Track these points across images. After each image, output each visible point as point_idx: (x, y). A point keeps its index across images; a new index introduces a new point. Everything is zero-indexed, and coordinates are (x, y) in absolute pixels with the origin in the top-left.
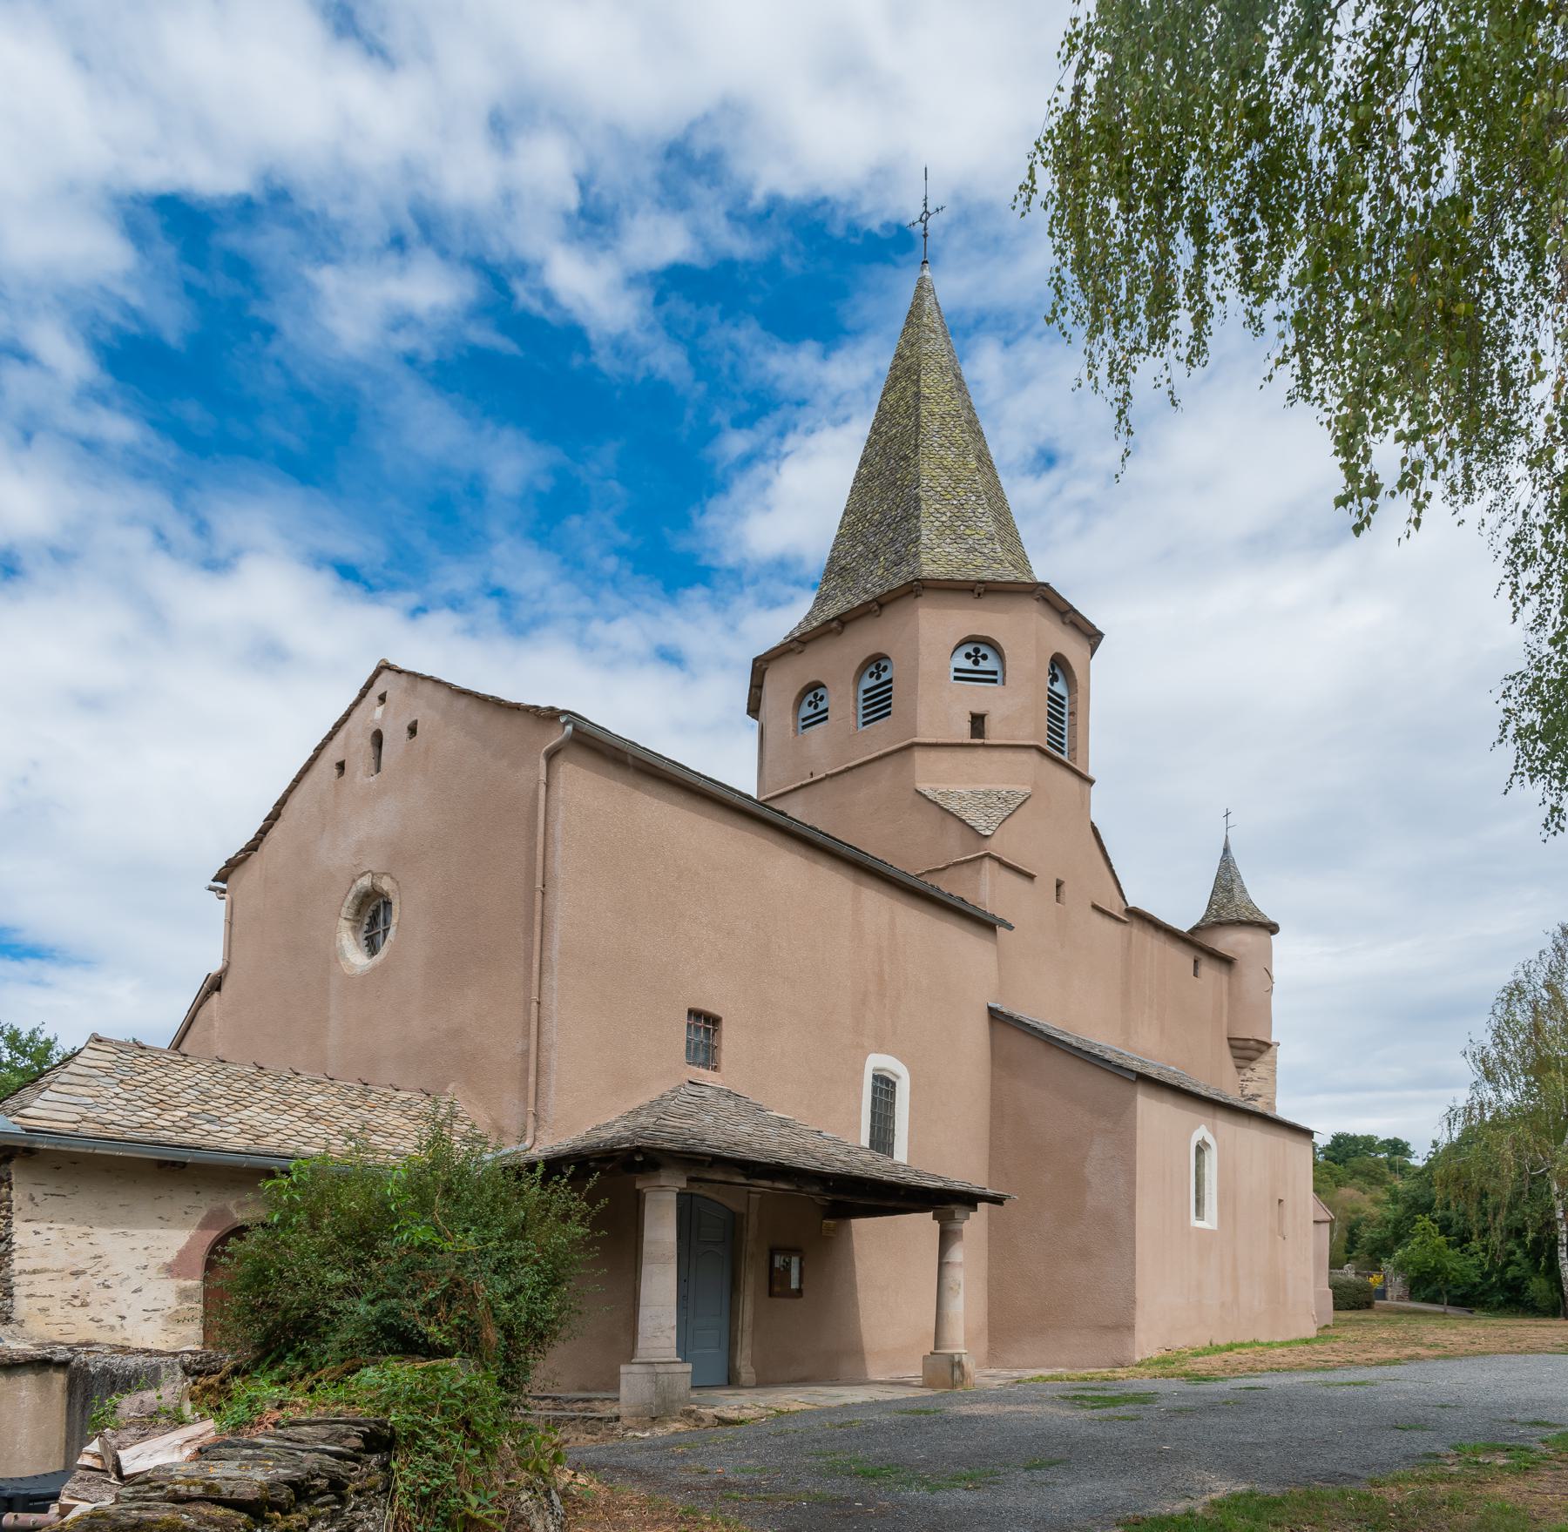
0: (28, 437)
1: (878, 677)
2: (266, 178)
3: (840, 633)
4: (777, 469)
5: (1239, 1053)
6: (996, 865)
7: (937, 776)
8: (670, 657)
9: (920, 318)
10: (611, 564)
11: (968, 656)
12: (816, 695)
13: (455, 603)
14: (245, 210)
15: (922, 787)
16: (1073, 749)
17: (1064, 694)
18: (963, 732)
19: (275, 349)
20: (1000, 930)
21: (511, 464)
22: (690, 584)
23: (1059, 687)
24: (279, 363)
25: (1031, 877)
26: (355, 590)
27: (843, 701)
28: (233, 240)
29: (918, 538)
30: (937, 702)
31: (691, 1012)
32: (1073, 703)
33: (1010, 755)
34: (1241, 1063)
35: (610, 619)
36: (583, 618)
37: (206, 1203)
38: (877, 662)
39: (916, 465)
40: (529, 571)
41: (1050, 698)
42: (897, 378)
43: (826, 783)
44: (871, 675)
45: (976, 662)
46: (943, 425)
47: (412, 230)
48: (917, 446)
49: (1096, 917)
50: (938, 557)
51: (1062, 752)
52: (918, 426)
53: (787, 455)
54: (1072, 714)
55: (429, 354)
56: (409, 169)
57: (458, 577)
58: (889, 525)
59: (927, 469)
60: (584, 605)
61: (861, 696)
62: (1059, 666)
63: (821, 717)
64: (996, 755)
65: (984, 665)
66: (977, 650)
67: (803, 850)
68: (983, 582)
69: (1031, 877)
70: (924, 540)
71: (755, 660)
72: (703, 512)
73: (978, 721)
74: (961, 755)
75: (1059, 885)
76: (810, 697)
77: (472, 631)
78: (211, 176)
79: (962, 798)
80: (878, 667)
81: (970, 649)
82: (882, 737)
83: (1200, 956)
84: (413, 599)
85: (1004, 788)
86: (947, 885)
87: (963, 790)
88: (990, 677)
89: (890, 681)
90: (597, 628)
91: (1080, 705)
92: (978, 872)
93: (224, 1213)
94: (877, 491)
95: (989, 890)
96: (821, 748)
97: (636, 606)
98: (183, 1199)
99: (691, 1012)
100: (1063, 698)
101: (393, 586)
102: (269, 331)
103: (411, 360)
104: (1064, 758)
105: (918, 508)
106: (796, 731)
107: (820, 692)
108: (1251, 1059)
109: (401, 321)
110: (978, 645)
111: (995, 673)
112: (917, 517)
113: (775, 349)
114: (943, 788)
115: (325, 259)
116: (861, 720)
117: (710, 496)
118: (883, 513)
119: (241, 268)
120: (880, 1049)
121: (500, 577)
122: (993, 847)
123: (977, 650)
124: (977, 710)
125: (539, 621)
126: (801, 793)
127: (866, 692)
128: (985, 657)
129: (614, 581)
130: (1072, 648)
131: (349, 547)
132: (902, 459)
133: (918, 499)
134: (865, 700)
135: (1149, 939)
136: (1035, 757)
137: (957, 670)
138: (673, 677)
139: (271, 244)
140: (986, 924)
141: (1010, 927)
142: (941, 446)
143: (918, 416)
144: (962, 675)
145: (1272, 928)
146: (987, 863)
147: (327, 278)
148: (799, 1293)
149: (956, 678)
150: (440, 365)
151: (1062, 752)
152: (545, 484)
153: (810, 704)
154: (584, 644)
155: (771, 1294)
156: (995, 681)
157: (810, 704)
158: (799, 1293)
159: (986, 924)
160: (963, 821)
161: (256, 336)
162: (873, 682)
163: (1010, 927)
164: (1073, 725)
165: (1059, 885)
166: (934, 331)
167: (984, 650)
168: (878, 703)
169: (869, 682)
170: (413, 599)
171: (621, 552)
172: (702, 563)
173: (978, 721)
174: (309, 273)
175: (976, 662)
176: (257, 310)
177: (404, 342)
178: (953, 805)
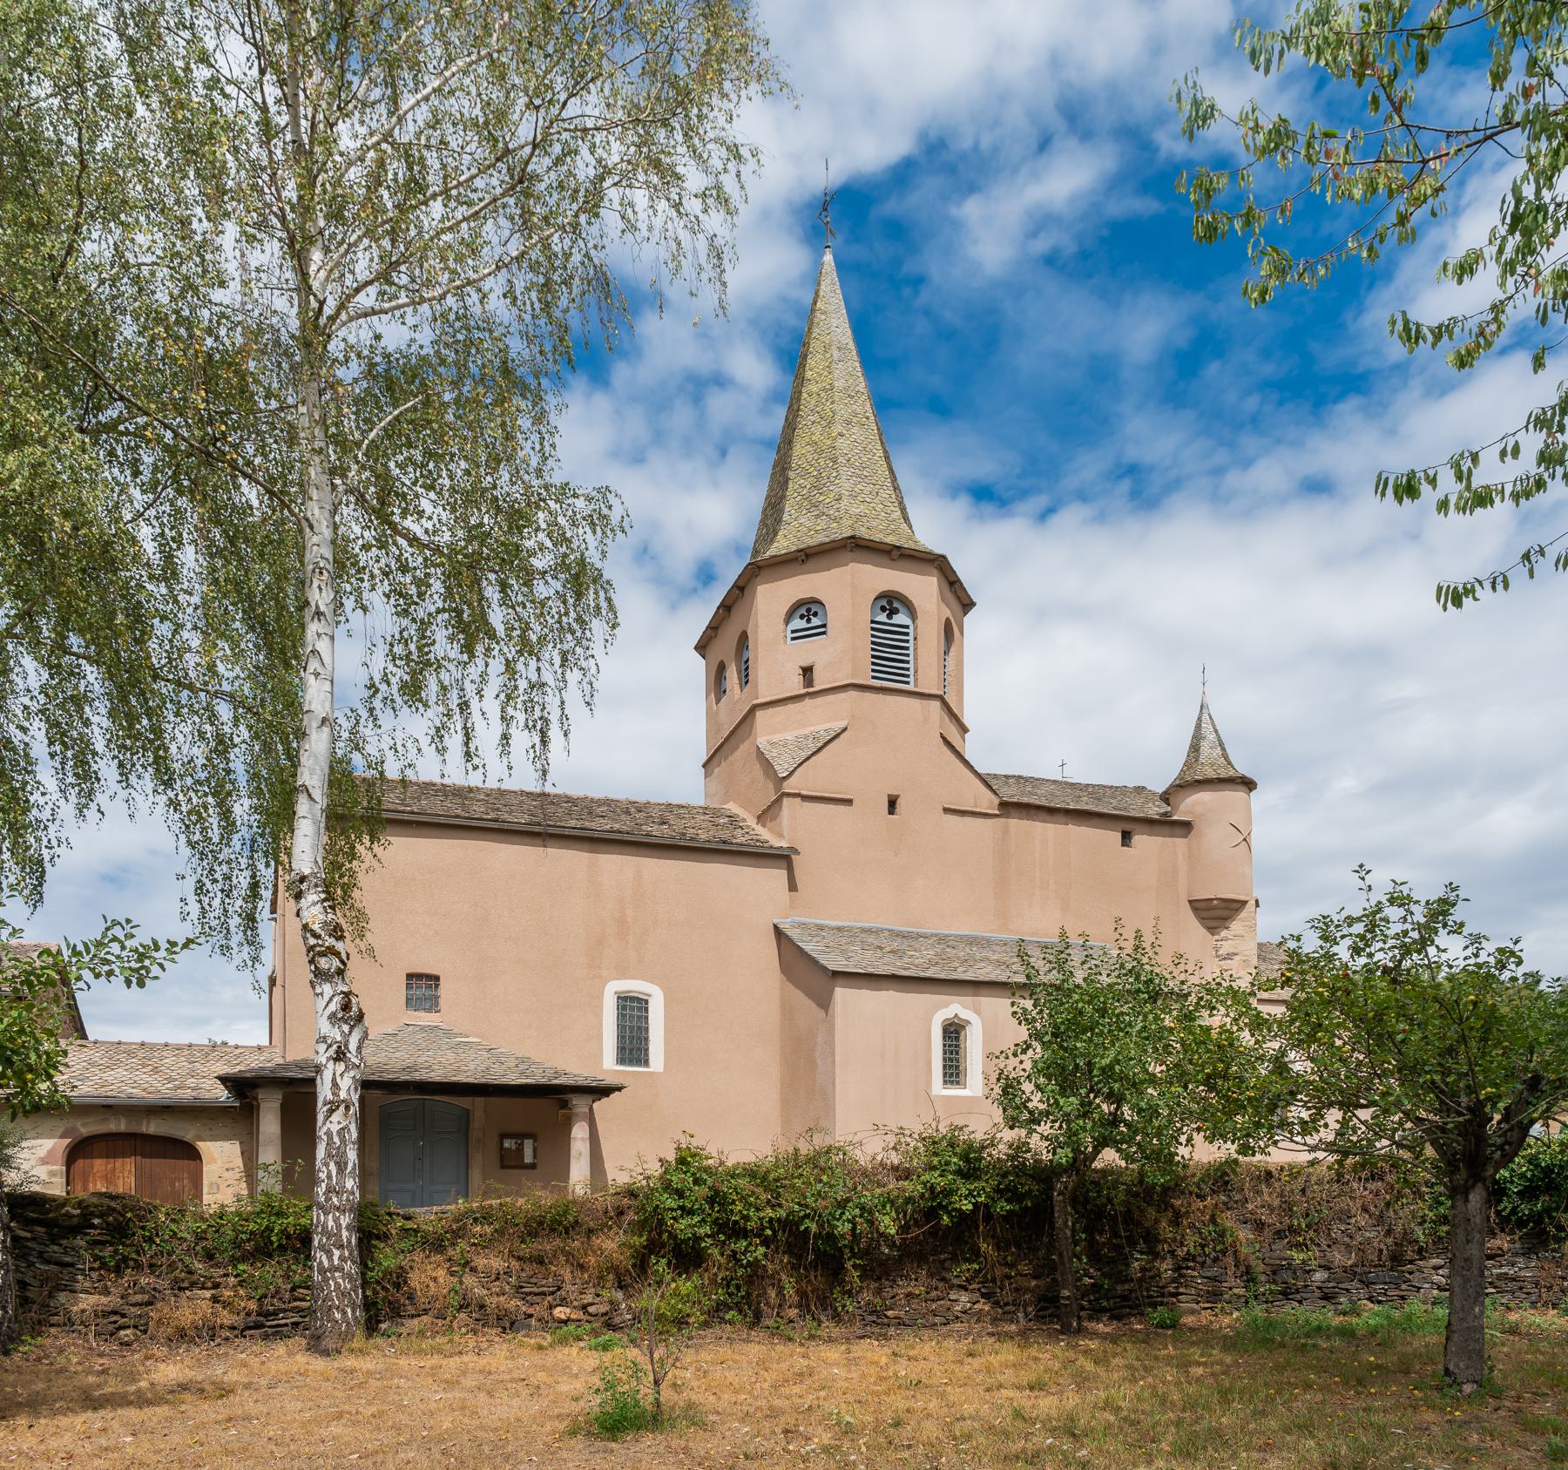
0: (723, 453)
1: (889, 616)
2: (923, 136)
4: (1454, 227)
5: (1205, 914)
8: (1318, 487)
10: (1252, 403)
13: (1083, 496)
14: (902, 174)
17: (907, 621)
18: (795, 685)
19: (925, 296)
21: (1146, 327)
22: (1340, 397)
24: (927, 312)
25: (849, 802)
26: (988, 508)
28: (891, 207)
31: (410, 976)
33: (831, 698)
34: (1212, 923)
35: (1247, 464)
36: (1218, 472)
37: (62, 1126)
40: (1152, 437)
45: (809, 621)
47: (1056, 122)
53: (1469, 205)
55: (1070, 248)
56: (1056, 61)
57: (1088, 466)
60: (1221, 456)
67: (527, 840)
69: (849, 802)
72: (1360, 313)
73: (807, 671)
75: (892, 804)
77: (1101, 518)
78: (872, 151)
83: (1128, 827)
89: (1383, 495)
90: (1233, 479)
93: (74, 1129)
97: (1279, 441)
98: (49, 1123)
99: (410, 976)
101: (1024, 494)
102: (918, 281)
103: (1050, 260)
108: (1226, 919)
109: (1041, 221)
113: (1463, 84)
115: (972, 188)
117: (1370, 287)
119: (897, 230)
120: (623, 974)
121: (1132, 454)
124: (804, 664)
125: (1174, 486)
128: (815, 614)
129: (1255, 421)
131: (984, 467)
138: (1323, 506)
139: (915, 202)
144: (798, 635)
145: (1248, 784)
147: (971, 209)
148: (533, 1166)
150: (1083, 255)
152: (1182, 339)
154: (1219, 499)
155: (503, 1167)
158: (533, 1166)
161: (907, 291)
165: (892, 804)
170: (1042, 501)
171: (1265, 385)
172: (1361, 369)
173: (807, 671)
174: (954, 211)
175: (809, 621)
176: (910, 267)
177: (1042, 245)
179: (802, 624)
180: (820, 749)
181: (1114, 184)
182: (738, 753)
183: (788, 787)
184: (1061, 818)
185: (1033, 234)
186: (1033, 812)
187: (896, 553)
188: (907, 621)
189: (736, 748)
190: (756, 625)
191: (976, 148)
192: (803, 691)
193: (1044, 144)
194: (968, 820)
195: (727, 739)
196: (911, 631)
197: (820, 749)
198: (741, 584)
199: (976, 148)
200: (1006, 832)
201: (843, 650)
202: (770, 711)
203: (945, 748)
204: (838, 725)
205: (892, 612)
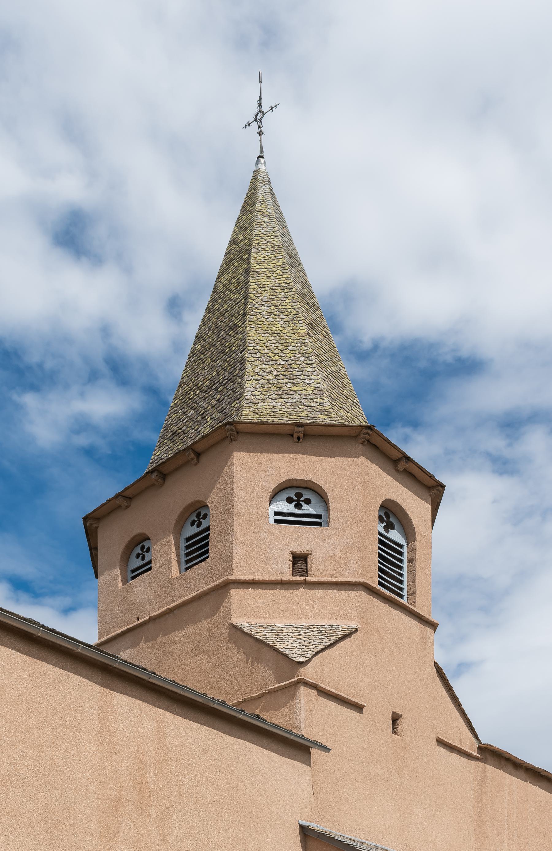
3: (161, 486)
6: (314, 692)
7: (248, 611)
9: (253, 204)
11: (289, 500)
12: (142, 548)
15: (237, 621)
16: (412, 593)
17: (401, 540)
18: (284, 570)
20: (314, 752)
23: (395, 535)
25: (358, 708)
27: (166, 553)
29: (242, 395)
30: (255, 538)
32: (412, 550)
38: (198, 512)
39: (244, 332)
41: (381, 542)
42: (230, 261)
43: (150, 626)
44: (193, 524)
45: (298, 506)
46: (273, 296)
48: (244, 315)
49: (443, 752)
50: (258, 403)
51: (401, 596)
52: (246, 297)
54: (410, 561)
56: (106, 331)
58: (216, 389)
59: (253, 334)
61: (183, 544)
62: (391, 514)
63: (146, 567)
64: (319, 593)
65: (307, 509)
66: (299, 495)
68: (301, 425)
69: (358, 708)
70: (248, 395)
71: (85, 519)
73: (300, 560)
74: (279, 593)
75: (395, 719)
76: (138, 550)
79: (279, 630)
80: (198, 515)
81: (292, 494)
82: (203, 578)
84: (67, 601)
85: (327, 622)
86: (274, 718)
87: (283, 623)
88: (317, 521)
89: (208, 529)
91: (418, 552)
92: (293, 697)
94: (209, 360)
95: (308, 715)
96: (147, 595)
100: (401, 546)
101: (53, 593)
103: (89, 452)
104: (404, 601)
105: (242, 368)
106: (125, 582)
107: (146, 544)
109: (82, 425)
110: (298, 491)
111: (319, 516)
112: (242, 377)
114: (262, 622)
115: (34, 388)
116: (184, 565)
118: (212, 380)
122: (306, 673)
123: (299, 495)
126: (129, 635)
127: (188, 539)
128: (308, 502)
130: (414, 505)
132: (231, 328)
133: (243, 362)
134: (187, 547)
135: (507, 776)
136: (363, 595)
137: (277, 513)
140: (299, 748)
141: (326, 749)
142: (270, 314)
143: (247, 289)
144: (281, 519)
146: (302, 689)
149: (276, 521)
151: (401, 596)
153: (138, 556)
156: (320, 524)
157: (138, 556)
159: (299, 748)
160: (276, 650)
162: (194, 530)
163: (326, 749)
164: (412, 571)
165: (395, 719)
166: (269, 216)
167: (306, 495)
168: (197, 549)
169: (192, 530)
170: (67, 601)
173: (300, 560)
174: (15, 397)
175: (298, 506)
177: (82, 440)
178: (269, 637)
179: (290, 508)
180: (336, 643)
181: (140, 419)
182: (181, 634)
183: (306, 673)
184: (522, 773)
185: (330, 319)
186: (503, 762)
187: (402, 465)
188: (401, 540)
189: (181, 627)
190: (230, 496)
191: (40, 366)
192: (288, 576)
193: (93, 377)
194: (455, 757)
195: (170, 611)
196: (405, 550)
197: (336, 643)
198: (199, 448)
199: (40, 366)
200: (484, 776)
201: (344, 545)
202: (250, 592)
203: (438, 679)
204: (349, 624)
205: (389, 527)
